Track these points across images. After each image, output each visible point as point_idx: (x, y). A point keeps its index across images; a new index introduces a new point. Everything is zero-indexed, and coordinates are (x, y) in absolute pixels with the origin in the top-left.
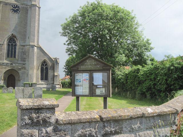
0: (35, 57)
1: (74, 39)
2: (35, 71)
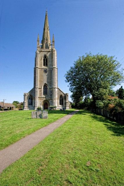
0: (56, 94)
1: (73, 83)
2: (56, 101)
